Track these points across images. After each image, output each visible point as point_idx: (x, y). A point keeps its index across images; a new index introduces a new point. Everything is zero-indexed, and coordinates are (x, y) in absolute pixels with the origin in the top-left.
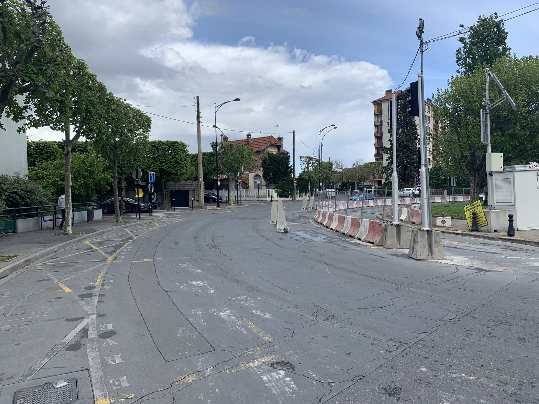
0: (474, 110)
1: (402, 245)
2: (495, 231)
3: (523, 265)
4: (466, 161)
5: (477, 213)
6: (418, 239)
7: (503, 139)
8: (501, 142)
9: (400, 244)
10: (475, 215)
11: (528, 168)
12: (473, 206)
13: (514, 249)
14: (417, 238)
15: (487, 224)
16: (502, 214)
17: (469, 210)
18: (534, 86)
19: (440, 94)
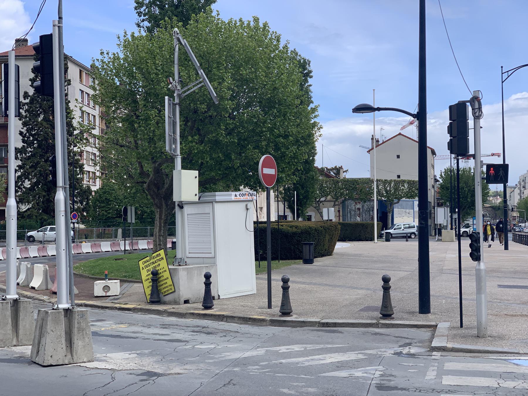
0: (158, 95)
1: (21, 340)
2: (186, 302)
3: (216, 358)
4: (147, 181)
5: (160, 271)
6: (48, 327)
7: (201, 148)
8: (198, 152)
9: (17, 336)
10: (155, 274)
11: (233, 198)
12: (153, 260)
13: (209, 330)
14: (46, 324)
15: (173, 290)
16: (196, 272)
17: (146, 266)
18: (244, 68)
19: (106, 60)
